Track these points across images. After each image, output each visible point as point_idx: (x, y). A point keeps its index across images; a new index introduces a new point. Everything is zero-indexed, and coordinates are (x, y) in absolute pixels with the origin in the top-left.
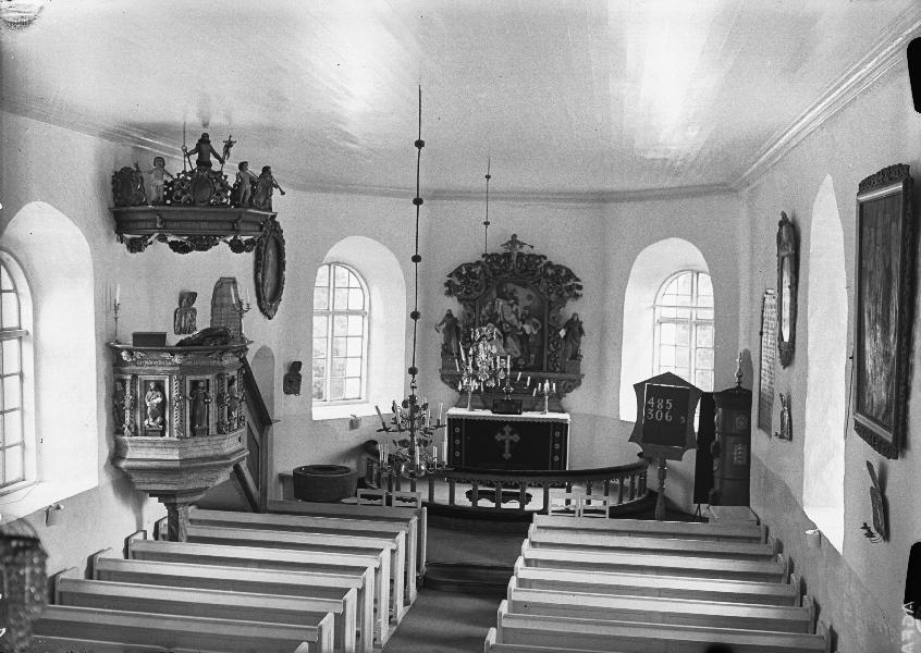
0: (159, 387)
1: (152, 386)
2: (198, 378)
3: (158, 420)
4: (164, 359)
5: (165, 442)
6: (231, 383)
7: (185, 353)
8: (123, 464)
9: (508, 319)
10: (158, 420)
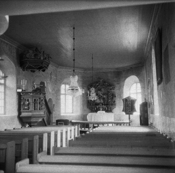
0: (28, 100)
1: (27, 100)
2: (36, 98)
3: (28, 107)
4: (29, 95)
5: (29, 111)
6: (42, 100)
7: (33, 93)
8: (21, 116)
9: (100, 95)
10: (28, 107)
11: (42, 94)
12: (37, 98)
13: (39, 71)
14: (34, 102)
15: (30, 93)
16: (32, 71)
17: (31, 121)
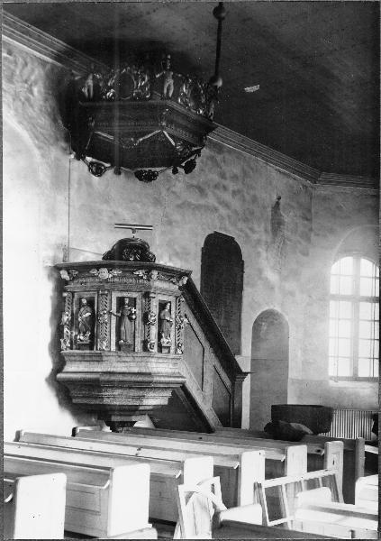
1: (84, 301)
2: (125, 294)
4: (93, 276)
11: (155, 273)
12: (134, 295)
13: (175, 172)
14: (118, 312)
15: (98, 266)
16: (139, 176)
17: (106, 401)
